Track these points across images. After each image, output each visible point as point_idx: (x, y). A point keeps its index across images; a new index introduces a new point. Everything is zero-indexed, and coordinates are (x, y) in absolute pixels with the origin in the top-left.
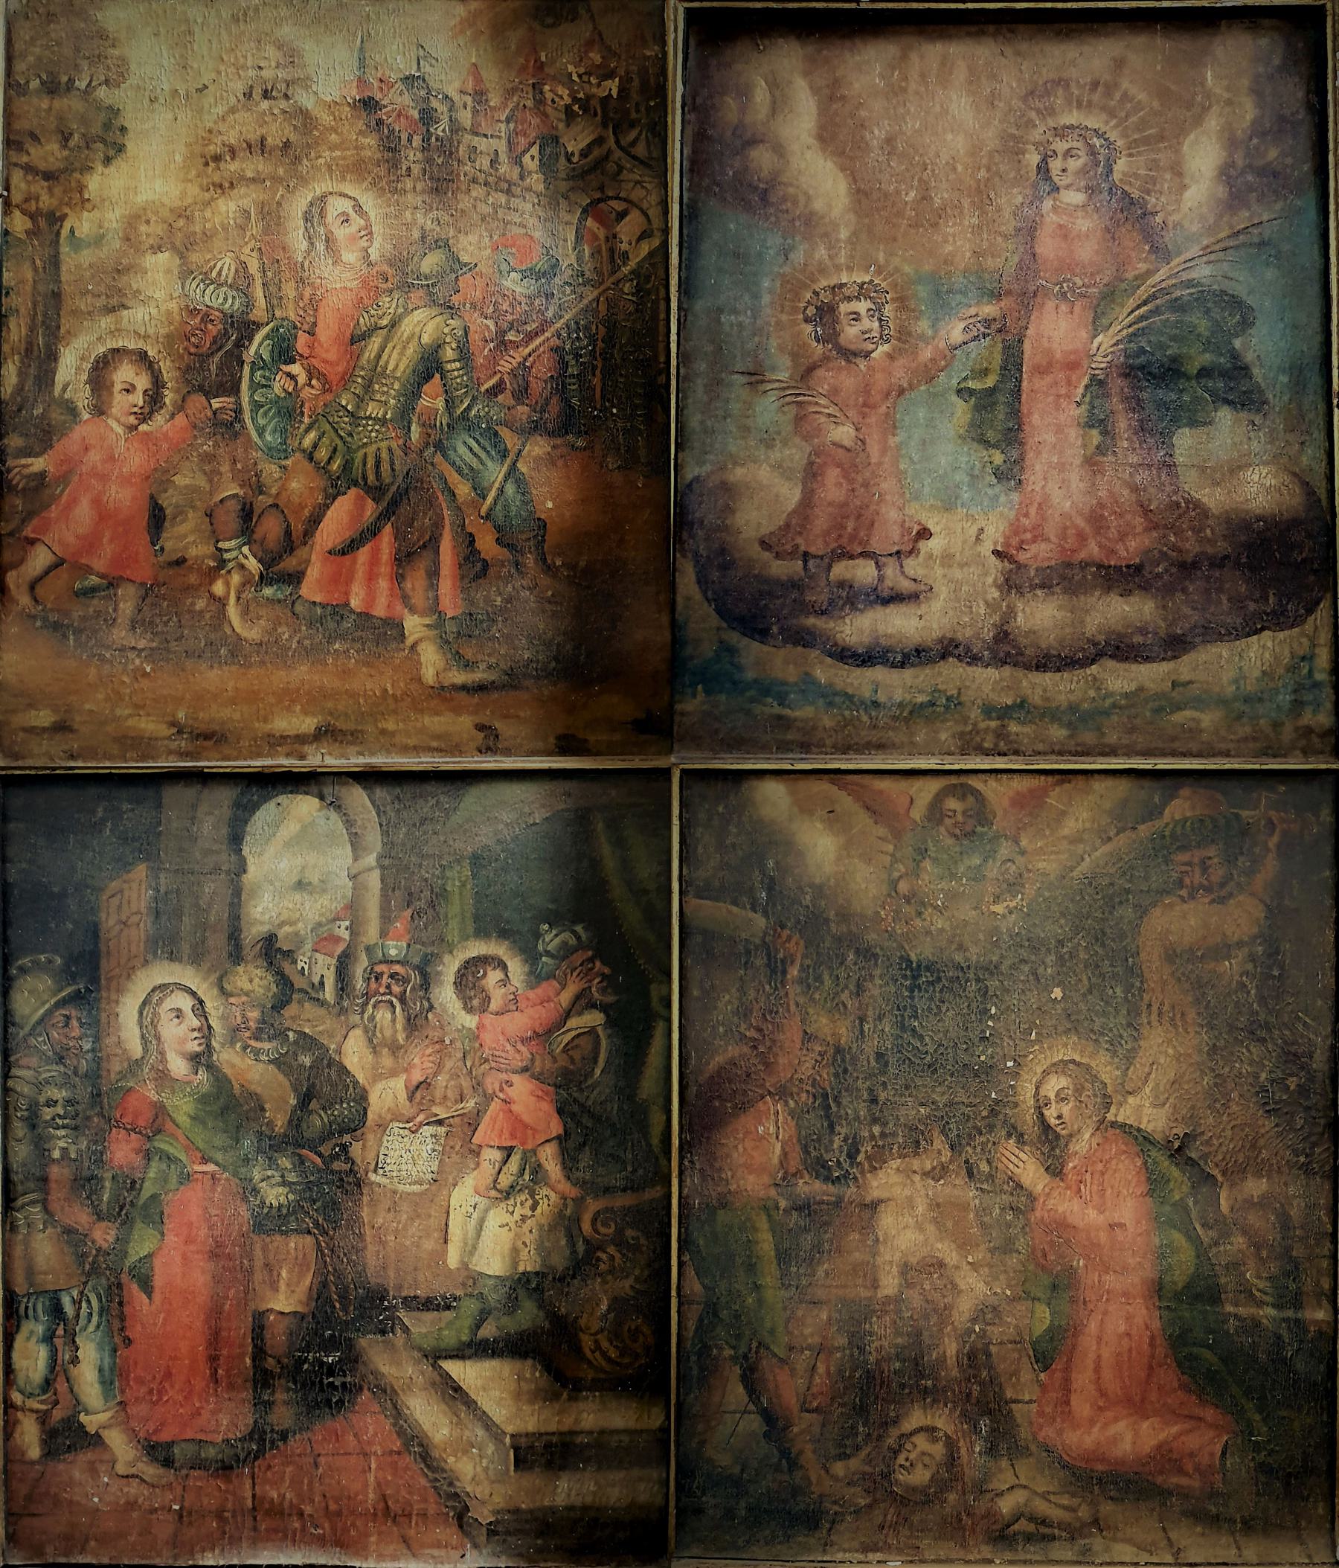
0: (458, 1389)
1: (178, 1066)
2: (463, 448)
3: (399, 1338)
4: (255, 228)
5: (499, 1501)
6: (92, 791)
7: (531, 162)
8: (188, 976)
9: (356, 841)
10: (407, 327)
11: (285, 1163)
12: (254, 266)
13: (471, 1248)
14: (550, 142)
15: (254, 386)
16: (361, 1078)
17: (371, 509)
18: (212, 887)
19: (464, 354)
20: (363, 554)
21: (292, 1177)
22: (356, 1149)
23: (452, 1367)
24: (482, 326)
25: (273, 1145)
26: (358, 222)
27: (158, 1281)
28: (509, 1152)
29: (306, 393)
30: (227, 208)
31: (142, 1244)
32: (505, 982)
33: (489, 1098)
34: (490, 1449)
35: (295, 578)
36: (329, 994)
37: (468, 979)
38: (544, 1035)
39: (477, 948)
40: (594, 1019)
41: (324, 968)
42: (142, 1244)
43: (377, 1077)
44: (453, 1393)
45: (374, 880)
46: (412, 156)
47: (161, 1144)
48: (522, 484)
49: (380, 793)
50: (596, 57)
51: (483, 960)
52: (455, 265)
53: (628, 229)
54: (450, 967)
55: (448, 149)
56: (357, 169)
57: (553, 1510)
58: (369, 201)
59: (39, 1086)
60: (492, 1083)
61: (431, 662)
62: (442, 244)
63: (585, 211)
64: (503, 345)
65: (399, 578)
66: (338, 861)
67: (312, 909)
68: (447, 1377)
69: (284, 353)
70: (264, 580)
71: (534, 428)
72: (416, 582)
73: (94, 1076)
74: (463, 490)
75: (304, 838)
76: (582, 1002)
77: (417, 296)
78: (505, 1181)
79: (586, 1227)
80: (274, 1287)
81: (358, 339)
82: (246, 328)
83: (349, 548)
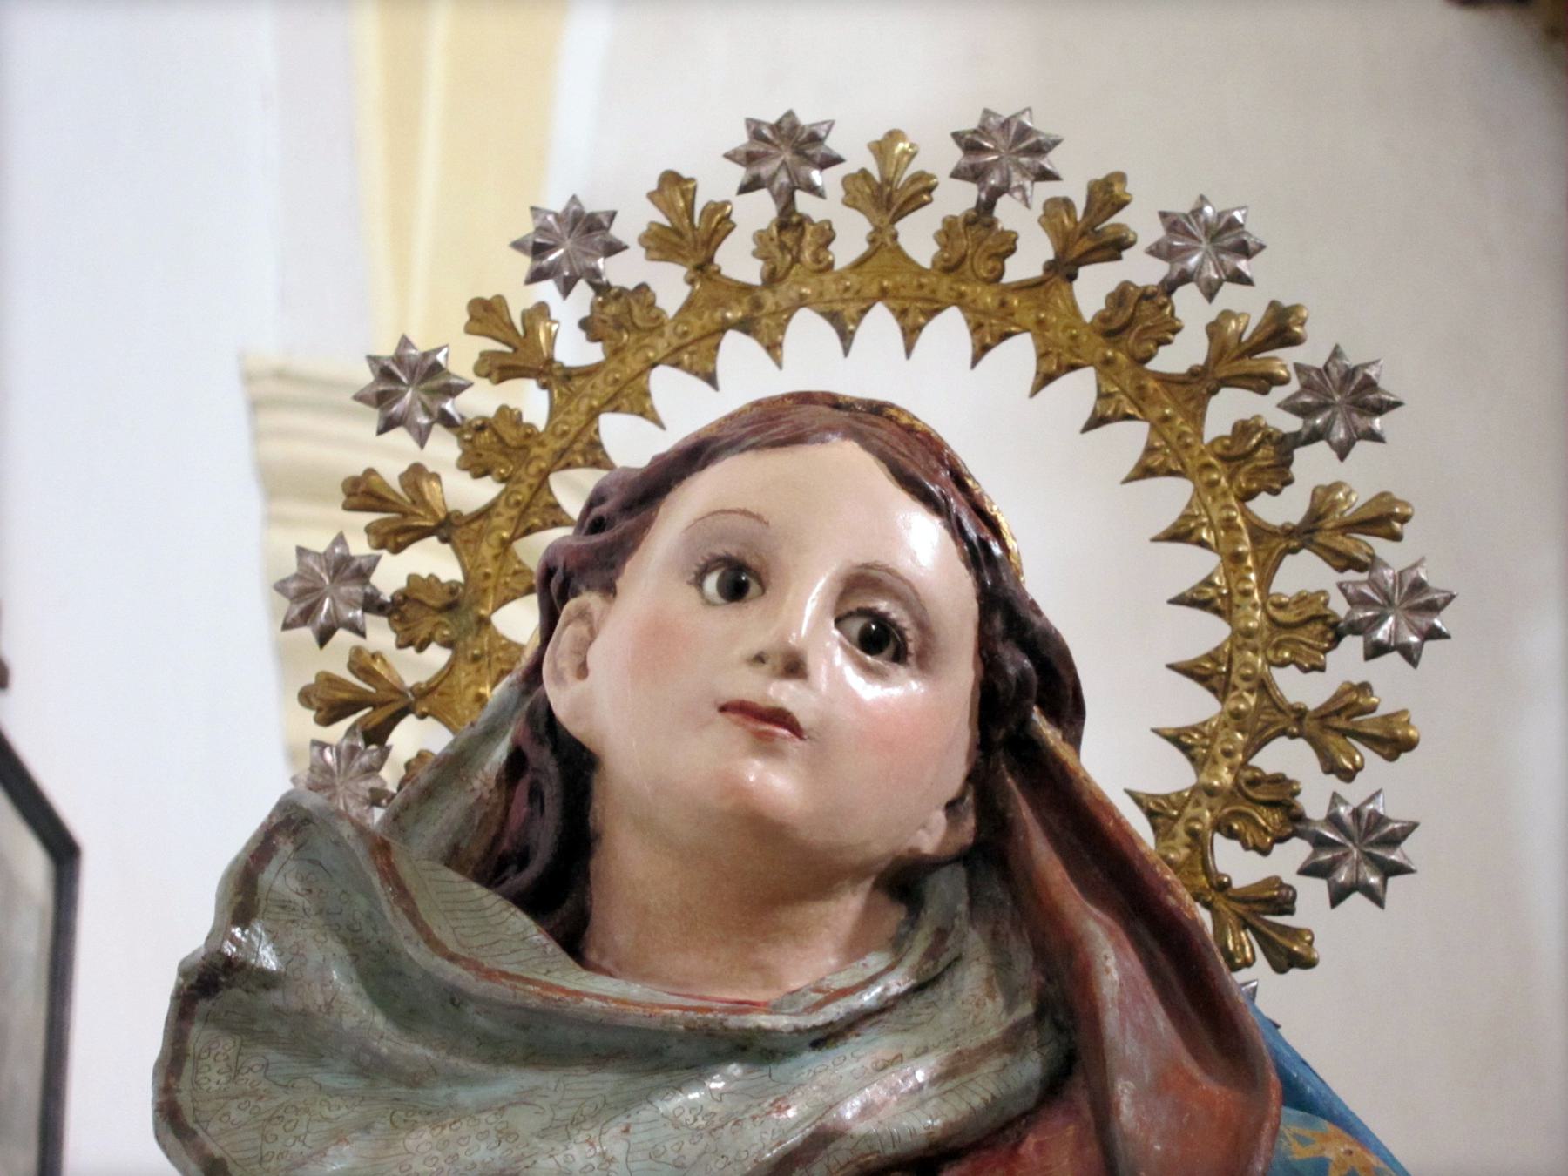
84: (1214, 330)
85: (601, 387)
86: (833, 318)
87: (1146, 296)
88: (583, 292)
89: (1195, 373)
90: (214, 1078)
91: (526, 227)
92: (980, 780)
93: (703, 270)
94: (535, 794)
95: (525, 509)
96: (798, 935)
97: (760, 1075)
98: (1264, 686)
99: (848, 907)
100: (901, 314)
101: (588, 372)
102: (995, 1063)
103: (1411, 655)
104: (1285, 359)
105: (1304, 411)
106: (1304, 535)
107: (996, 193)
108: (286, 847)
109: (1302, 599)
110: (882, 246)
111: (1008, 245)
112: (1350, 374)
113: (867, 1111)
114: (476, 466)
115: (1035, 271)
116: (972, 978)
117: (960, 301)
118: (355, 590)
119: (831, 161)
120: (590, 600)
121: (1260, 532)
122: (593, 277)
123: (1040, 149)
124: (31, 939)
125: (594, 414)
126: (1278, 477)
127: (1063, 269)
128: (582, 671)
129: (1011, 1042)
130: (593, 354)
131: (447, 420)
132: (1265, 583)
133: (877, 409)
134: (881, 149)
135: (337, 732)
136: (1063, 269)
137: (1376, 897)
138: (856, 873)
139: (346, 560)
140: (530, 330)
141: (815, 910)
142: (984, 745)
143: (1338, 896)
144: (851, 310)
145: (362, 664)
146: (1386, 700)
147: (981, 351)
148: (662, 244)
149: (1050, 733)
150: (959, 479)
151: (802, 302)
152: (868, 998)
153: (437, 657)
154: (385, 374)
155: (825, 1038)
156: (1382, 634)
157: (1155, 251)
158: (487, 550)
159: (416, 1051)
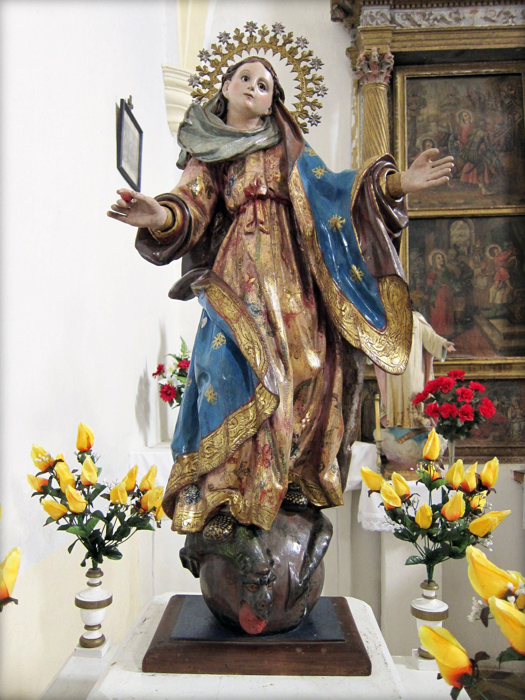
0: (492, 325)
1: (439, 267)
2: (488, 154)
3: (481, 315)
4: (450, 117)
5: (501, 345)
6: (424, 221)
7: (499, 105)
8: (441, 252)
9: (470, 229)
10: (479, 133)
11: (459, 284)
12: (450, 125)
13: (494, 298)
14: (502, 103)
15: (451, 145)
16: (472, 268)
17: (472, 165)
18: (445, 236)
19: (488, 138)
20: (471, 173)
21: (460, 286)
22: (472, 281)
23: (492, 321)
24: (491, 133)
25: (456, 281)
26: (468, 116)
27: (436, 305)
28: (500, 281)
29: (460, 146)
30: (445, 115)
31: (433, 299)
32: (498, 251)
33: (496, 272)
34: (499, 336)
35: (459, 178)
36: (466, 254)
37: (491, 251)
38: (506, 260)
39: (492, 246)
40: (514, 258)
41: (465, 249)
42: (433, 299)
43: (476, 268)
44: (491, 326)
45: (474, 234)
46: (477, 105)
47: (436, 281)
48: (499, 161)
49: (474, 220)
50: (510, 87)
51: (494, 248)
52: (486, 123)
53: (517, 116)
54: (488, 249)
55: (484, 103)
56: (468, 107)
57: (511, 347)
58: (470, 114)
59: (415, 271)
60: (497, 269)
61: (484, 191)
62: (483, 120)
63: (509, 114)
64: (495, 136)
65: (478, 177)
66: (467, 232)
67: (462, 239)
68: (490, 323)
69: (456, 139)
70: (454, 178)
71: (501, 151)
72: (480, 178)
73: (424, 269)
74: (489, 162)
75: (461, 228)
76: (512, 255)
77: (480, 129)
78: (500, 286)
79: (515, 294)
80: (458, 307)
81: (469, 136)
82: (449, 135)
83: (468, 173)
84: (302, 53)
85: (228, 56)
86: (256, 49)
87: (294, 48)
88: (226, 44)
89: (300, 59)
90: (184, 137)
91: (219, 35)
92: (272, 106)
93: (241, 42)
94: (221, 105)
95: (218, 72)
96: (251, 123)
97: (246, 139)
98: (305, 99)
99: (257, 120)
100: (265, 49)
101: (227, 54)
102: (273, 138)
103: (323, 96)
104: (310, 58)
105: (312, 65)
106: (311, 80)
107: (277, 34)
108: (192, 109)
109: (310, 88)
110: (263, 40)
111: (278, 41)
112: (318, 60)
113: (259, 142)
114: (212, 66)
115: (281, 44)
116: (271, 129)
117: (272, 48)
118: (197, 81)
119: (257, 28)
120: (228, 81)
121: (306, 80)
122: (227, 42)
123: (283, 28)
124: (137, 144)
125: (227, 60)
126: (309, 73)
127: (284, 44)
128: (227, 90)
129: (275, 136)
130: (227, 52)
131: (209, 60)
132: (306, 86)
133: (263, 59)
134: (263, 27)
135: (195, 99)
136: (284, 44)
137: (316, 125)
138: (259, 116)
139: (196, 77)
140: (219, 49)
141: (254, 120)
142: (273, 102)
143: (312, 125)
144: (258, 48)
145: (198, 91)
146: (319, 102)
147: (274, 55)
148: (236, 38)
149: (281, 101)
150: (272, 68)
151: (252, 47)
152: (259, 130)
153: (207, 90)
154: (201, 53)
155: (254, 135)
156: (320, 93)
157: (296, 43)
158: (213, 77)
159: (207, 134)
